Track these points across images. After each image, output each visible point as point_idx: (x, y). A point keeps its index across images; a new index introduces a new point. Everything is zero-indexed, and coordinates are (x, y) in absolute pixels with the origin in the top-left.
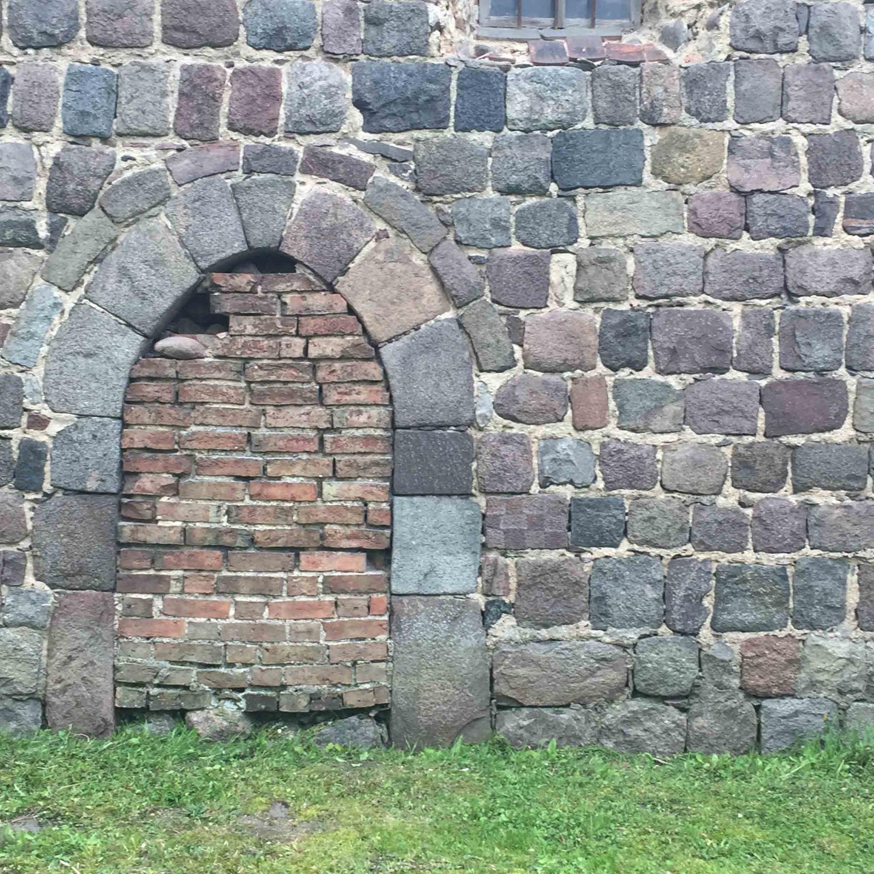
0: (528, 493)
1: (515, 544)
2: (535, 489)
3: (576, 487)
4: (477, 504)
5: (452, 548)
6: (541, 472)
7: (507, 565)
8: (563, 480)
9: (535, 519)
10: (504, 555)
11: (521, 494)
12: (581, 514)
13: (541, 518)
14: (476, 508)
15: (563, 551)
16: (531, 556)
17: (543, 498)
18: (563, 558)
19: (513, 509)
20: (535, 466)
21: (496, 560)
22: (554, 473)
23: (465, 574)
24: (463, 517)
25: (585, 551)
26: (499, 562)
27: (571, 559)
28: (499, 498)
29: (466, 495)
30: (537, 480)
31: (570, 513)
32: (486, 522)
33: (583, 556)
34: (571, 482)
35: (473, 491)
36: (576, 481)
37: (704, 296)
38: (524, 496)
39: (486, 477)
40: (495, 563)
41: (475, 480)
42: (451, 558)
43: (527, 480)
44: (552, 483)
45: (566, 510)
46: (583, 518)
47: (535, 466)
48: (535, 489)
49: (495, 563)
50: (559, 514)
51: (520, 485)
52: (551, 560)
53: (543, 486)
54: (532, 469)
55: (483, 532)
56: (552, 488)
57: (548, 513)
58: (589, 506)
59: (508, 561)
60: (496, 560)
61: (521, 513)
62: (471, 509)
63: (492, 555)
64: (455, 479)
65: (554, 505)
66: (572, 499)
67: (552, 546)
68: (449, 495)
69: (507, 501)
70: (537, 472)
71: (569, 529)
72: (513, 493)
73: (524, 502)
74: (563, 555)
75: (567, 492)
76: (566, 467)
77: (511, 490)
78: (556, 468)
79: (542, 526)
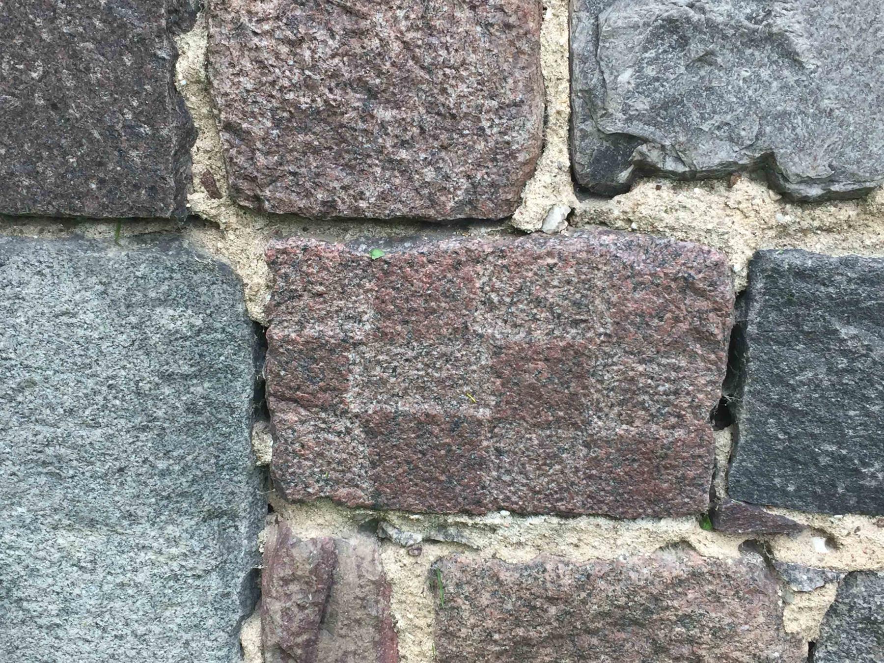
0: (504, 224)
1: (427, 476)
2: (547, 199)
3: (786, 197)
4: (227, 275)
5: (98, 500)
6: (588, 101)
7: (383, 586)
8: (723, 154)
9: (536, 372)
10: (374, 527)
11: (465, 224)
12: (801, 351)
13: (572, 364)
14: (218, 293)
15: (687, 528)
16: (511, 544)
17: (588, 261)
18: (674, 564)
19: (412, 311)
20: (554, 65)
21: (329, 556)
22: (668, 111)
23: (175, 617)
24: (144, 345)
25: (793, 530)
26: (348, 573)
27: (718, 570)
28: (333, 247)
29: (160, 220)
30: (557, 153)
31: (737, 338)
32: (277, 374)
33: (787, 551)
34: (766, 170)
35: (199, 201)
36: (796, 165)
37: (716, 117)
38: (482, 240)
39: (258, 128)
40: (326, 568)
41: (203, 143)
42: (96, 539)
43: (503, 152)
44: (647, 171)
45: (718, 329)
46: (810, 372)
47: (554, 65)
48: (547, 199)
49: (326, 568)
50: (677, 346)
51: (456, 180)
52: (615, 572)
53: (593, 182)
54: (536, 83)
55: (261, 411)
56: (648, 199)
57: (616, 338)
58: (850, 309)
59: (391, 562)
60: (329, 556)
61: (463, 333)
62: (191, 299)
63: (311, 530)
64: (79, 134)
65: (640, 299)
66: (756, 261)
67: (633, 487)
68: (68, 221)
69: (386, 271)
70: (560, 103)
71: (724, 416)
72: (422, 224)
73: (481, 276)
74: (684, 544)
75: (734, 225)
76: (742, 77)
77: (408, 203)
78: (679, 77)
79: (572, 402)
